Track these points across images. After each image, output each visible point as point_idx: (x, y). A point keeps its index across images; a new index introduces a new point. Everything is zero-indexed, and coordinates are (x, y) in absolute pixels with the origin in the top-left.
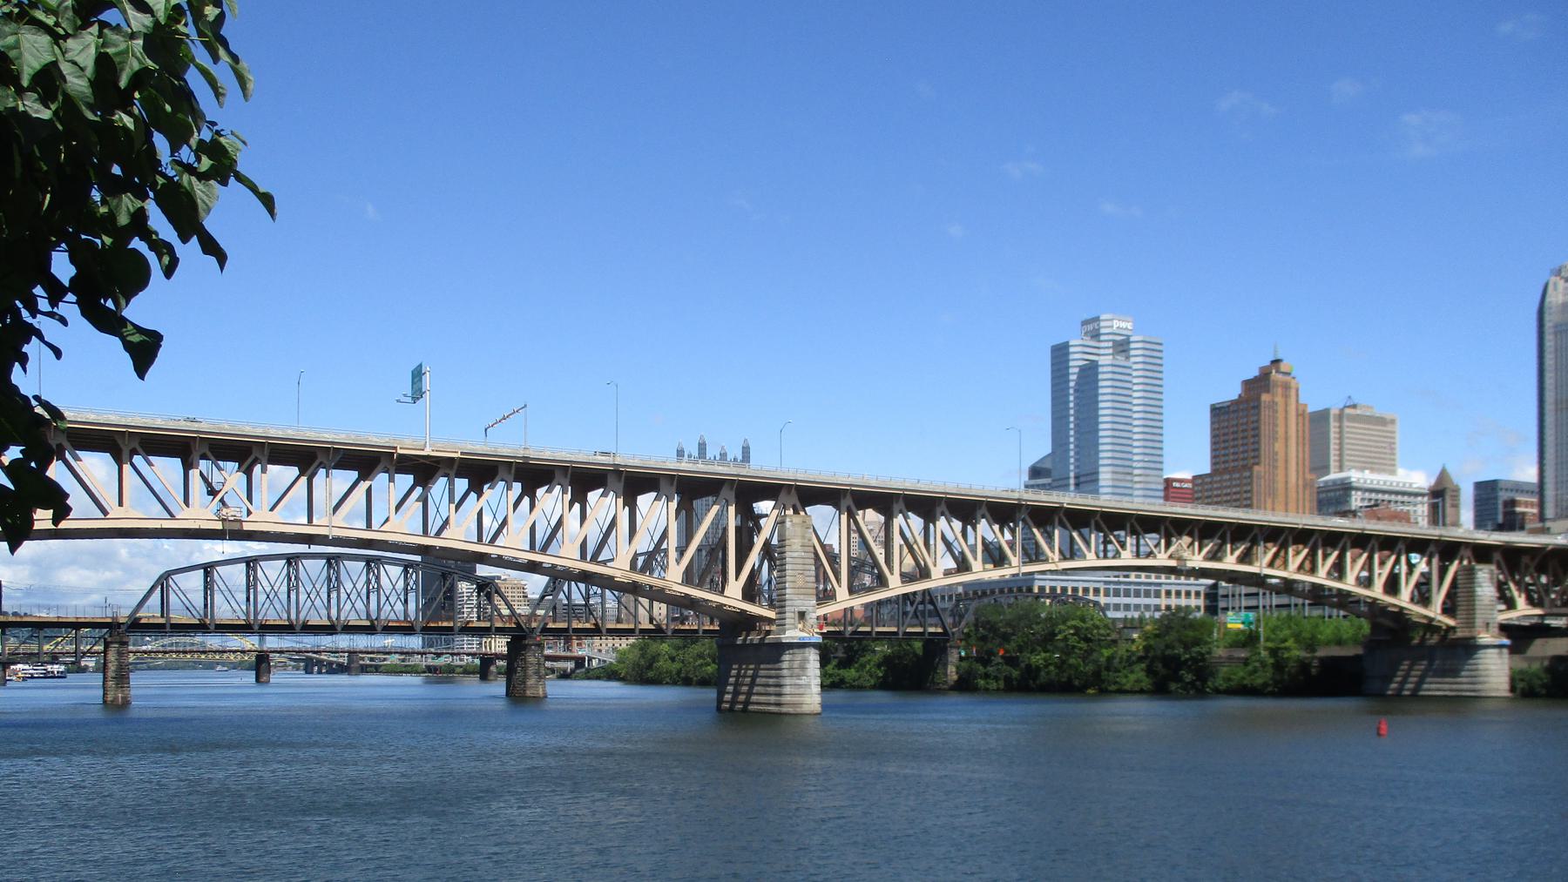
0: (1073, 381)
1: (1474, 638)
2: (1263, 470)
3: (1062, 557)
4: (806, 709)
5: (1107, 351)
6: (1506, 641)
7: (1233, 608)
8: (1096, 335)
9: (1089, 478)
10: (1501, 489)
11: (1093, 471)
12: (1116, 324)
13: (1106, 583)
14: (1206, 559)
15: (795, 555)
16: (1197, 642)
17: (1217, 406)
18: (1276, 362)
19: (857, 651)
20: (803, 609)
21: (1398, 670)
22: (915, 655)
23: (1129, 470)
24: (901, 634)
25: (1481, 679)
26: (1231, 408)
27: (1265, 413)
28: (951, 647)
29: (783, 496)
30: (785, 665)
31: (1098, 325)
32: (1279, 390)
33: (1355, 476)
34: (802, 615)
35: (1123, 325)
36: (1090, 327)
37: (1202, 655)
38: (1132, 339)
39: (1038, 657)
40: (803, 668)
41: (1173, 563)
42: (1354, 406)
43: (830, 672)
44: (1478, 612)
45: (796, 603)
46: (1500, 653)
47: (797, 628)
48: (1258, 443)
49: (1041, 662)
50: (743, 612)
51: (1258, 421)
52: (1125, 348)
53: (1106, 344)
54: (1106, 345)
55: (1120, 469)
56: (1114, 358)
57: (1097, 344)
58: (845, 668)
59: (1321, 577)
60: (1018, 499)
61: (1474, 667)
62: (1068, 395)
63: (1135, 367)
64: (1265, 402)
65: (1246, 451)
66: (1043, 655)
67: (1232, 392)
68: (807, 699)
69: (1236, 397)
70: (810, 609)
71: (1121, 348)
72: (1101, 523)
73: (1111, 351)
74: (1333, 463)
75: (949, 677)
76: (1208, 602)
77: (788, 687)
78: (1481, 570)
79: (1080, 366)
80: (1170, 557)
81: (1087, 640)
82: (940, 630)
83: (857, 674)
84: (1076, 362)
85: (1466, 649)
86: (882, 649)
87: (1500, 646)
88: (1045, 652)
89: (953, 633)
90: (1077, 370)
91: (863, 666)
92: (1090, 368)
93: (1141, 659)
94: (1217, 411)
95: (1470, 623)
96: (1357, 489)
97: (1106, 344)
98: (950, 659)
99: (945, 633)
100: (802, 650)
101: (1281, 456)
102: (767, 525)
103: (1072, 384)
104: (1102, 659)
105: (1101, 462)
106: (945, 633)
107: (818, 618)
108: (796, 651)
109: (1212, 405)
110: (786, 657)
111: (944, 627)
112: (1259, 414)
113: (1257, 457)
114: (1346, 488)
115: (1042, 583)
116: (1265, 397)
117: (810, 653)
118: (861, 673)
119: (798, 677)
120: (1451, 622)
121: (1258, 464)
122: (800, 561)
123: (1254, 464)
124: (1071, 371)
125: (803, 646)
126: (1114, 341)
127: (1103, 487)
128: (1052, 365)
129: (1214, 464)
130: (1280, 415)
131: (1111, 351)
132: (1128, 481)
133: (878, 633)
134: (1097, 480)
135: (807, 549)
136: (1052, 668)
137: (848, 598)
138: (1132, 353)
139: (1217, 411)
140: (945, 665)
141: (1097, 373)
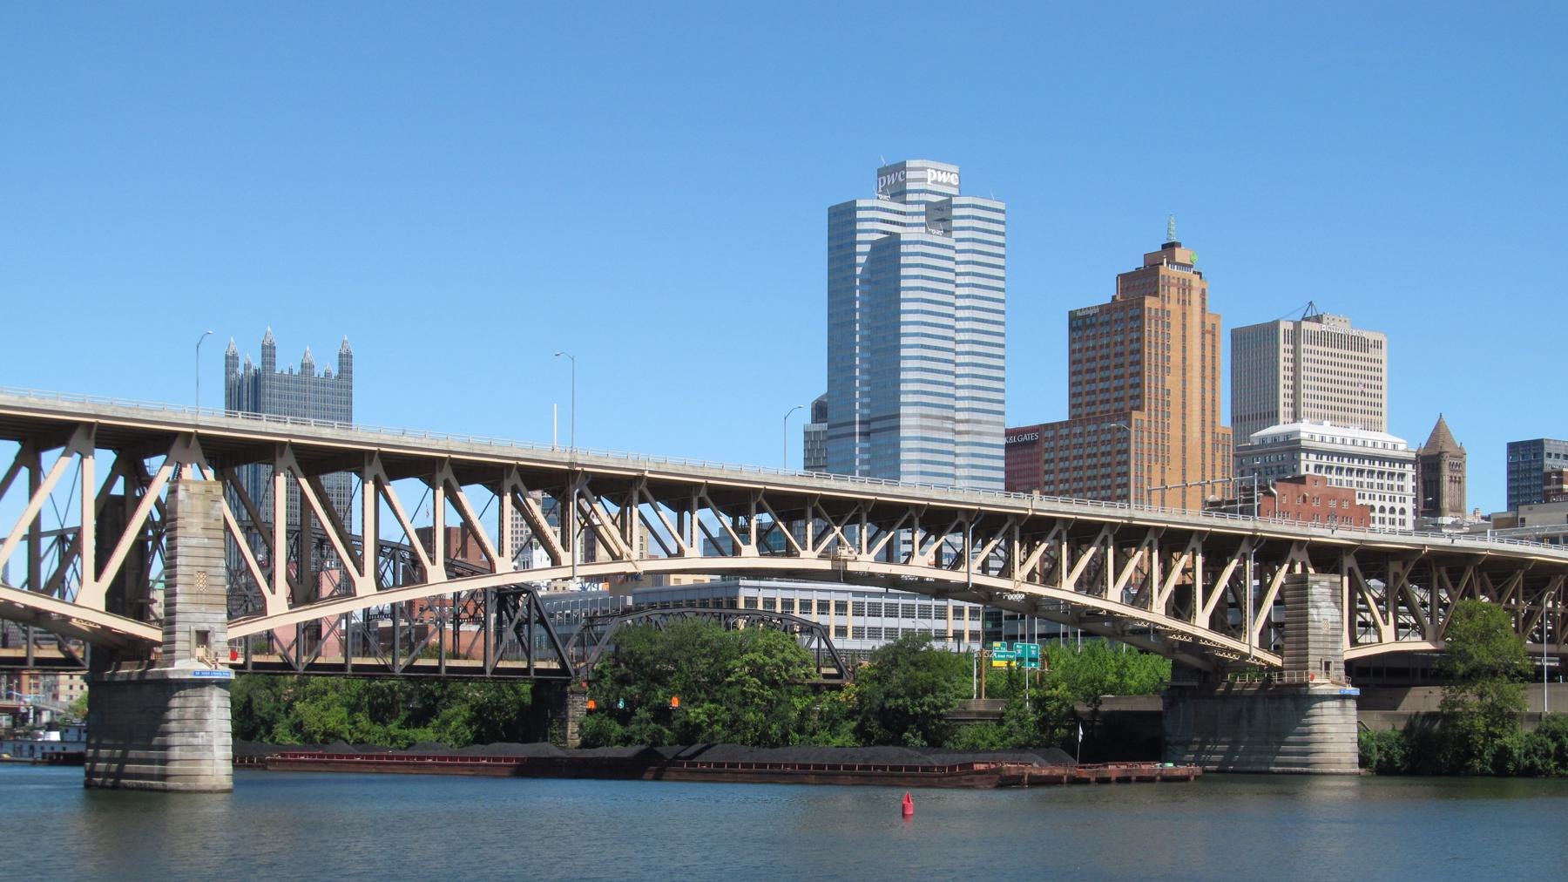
0: (860, 265)
1: (1307, 684)
2: (1146, 419)
3: (884, 555)
4: (204, 783)
5: (916, 220)
6: (1355, 691)
7: (1023, 637)
8: (899, 193)
9: (885, 424)
10: (1549, 455)
11: (893, 413)
12: (931, 175)
13: (855, 594)
14: (877, 560)
15: (194, 542)
16: (931, 688)
17: (1079, 314)
18: (1170, 247)
19: (442, 697)
20: (205, 627)
21: (169, 709)
22: (521, 704)
23: (950, 413)
24: (488, 671)
25: (1315, 747)
26: (1101, 319)
27: (1150, 328)
28: (572, 693)
29: (177, 448)
30: (173, 714)
31: (904, 176)
32: (1174, 290)
33: (1307, 430)
34: (203, 637)
35: (943, 178)
36: (891, 179)
37: (937, 708)
38: (955, 201)
39: (699, 710)
40: (200, 720)
41: (826, 565)
42: (1318, 319)
43: (394, 733)
44: (1311, 645)
45: (193, 617)
46: (1343, 708)
47: (192, 656)
48: (1140, 374)
49: (702, 717)
50: (106, 629)
51: (1140, 340)
52: (944, 215)
53: (915, 208)
54: (914, 206)
55: (934, 411)
56: (926, 230)
57: (901, 207)
58: (417, 726)
59: (1066, 591)
60: (570, 464)
61: (1306, 729)
62: (854, 288)
63: (959, 246)
64: (1150, 309)
65: (1122, 388)
66: (706, 705)
67: (1101, 292)
68: (206, 768)
69: (1108, 300)
70: (217, 627)
71: (939, 215)
72: (764, 502)
73: (923, 219)
74: (1284, 410)
75: (569, 741)
76: (989, 625)
77: (177, 748)
78: (1317, 582)
79: (872, 243)
80: (820, 557)
81: (774, 684)
82: (555, 666)
83: (437, 736)
84: (868, 234)
85: (1299, 699)
86: (475, 693)
87: (1343, 697)
88: (712, 702)
89: (577, 672)
90: (867, 248)
91: (446, 723)
92: (888, 246)
93: (851, 715)
94: (1080, 324)
95: (1301, 663)
96: (1308, 451)
97: (915, 208)
98: (570, 713)
99: (564, 670)
100: (198, 691)
101: (1176, 399)
102: (158, 489)
103: (859, 270)
104: (794, 715)
105: (903, 399)
106: (564, 670)
107: (231, 642)
108: (189, 692)
109: (1070, 313)
110: (175, 702)
111: (562, 663)
112: (1141, 328)
113: (1140, 397)
114: (1292, 447)
115: (752, 593)
116: (1149, 302)
117: (211, 695)
118: (442, 734)
119: (192, 732)
120: (1276, 661)
121: (1140, 408)
122: (201, 552)
123: (1132, 408)
124: (859, 248)
125: (200, 684)
126: (928, 204)
127: (906, 438)
128: (830, 238)
129: (1072, 406)
130: (1176, 331)
131: (923, 219)
132: (947, 430)
133: (450, 669)
134: (898, 428)
135: (212, 533)
136: (718, 728)
137: (288, 611)
138: (956, 223)
139: (1080, 324)
140: (563, 724)
141: (898, 255)
